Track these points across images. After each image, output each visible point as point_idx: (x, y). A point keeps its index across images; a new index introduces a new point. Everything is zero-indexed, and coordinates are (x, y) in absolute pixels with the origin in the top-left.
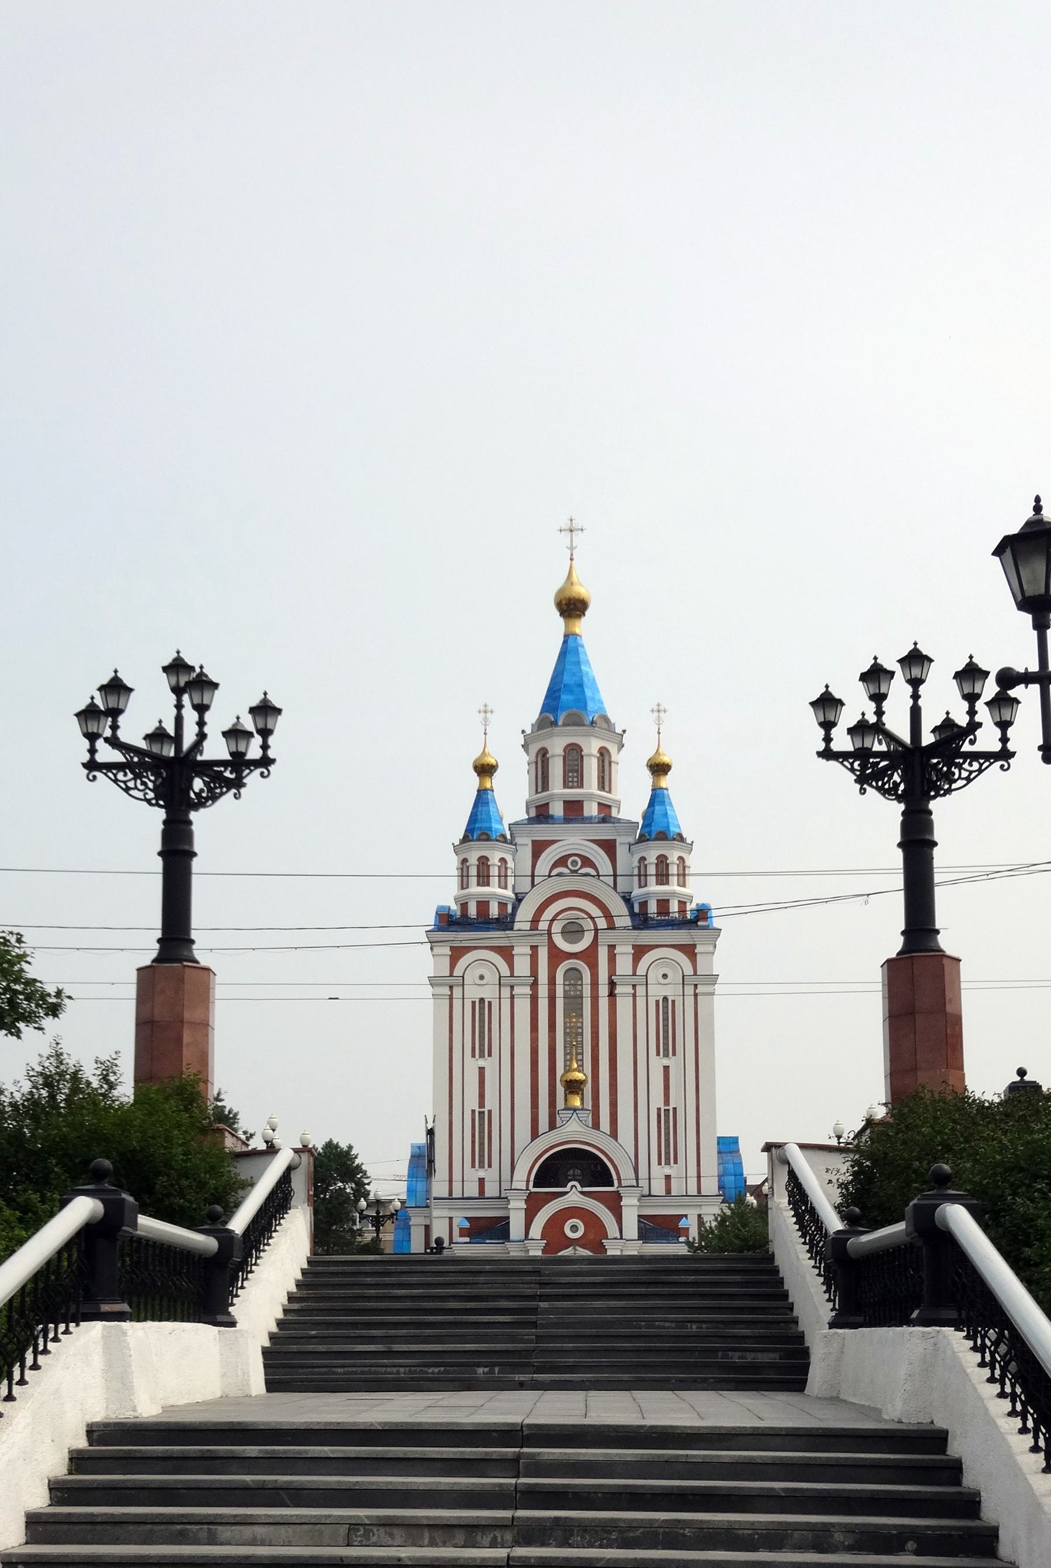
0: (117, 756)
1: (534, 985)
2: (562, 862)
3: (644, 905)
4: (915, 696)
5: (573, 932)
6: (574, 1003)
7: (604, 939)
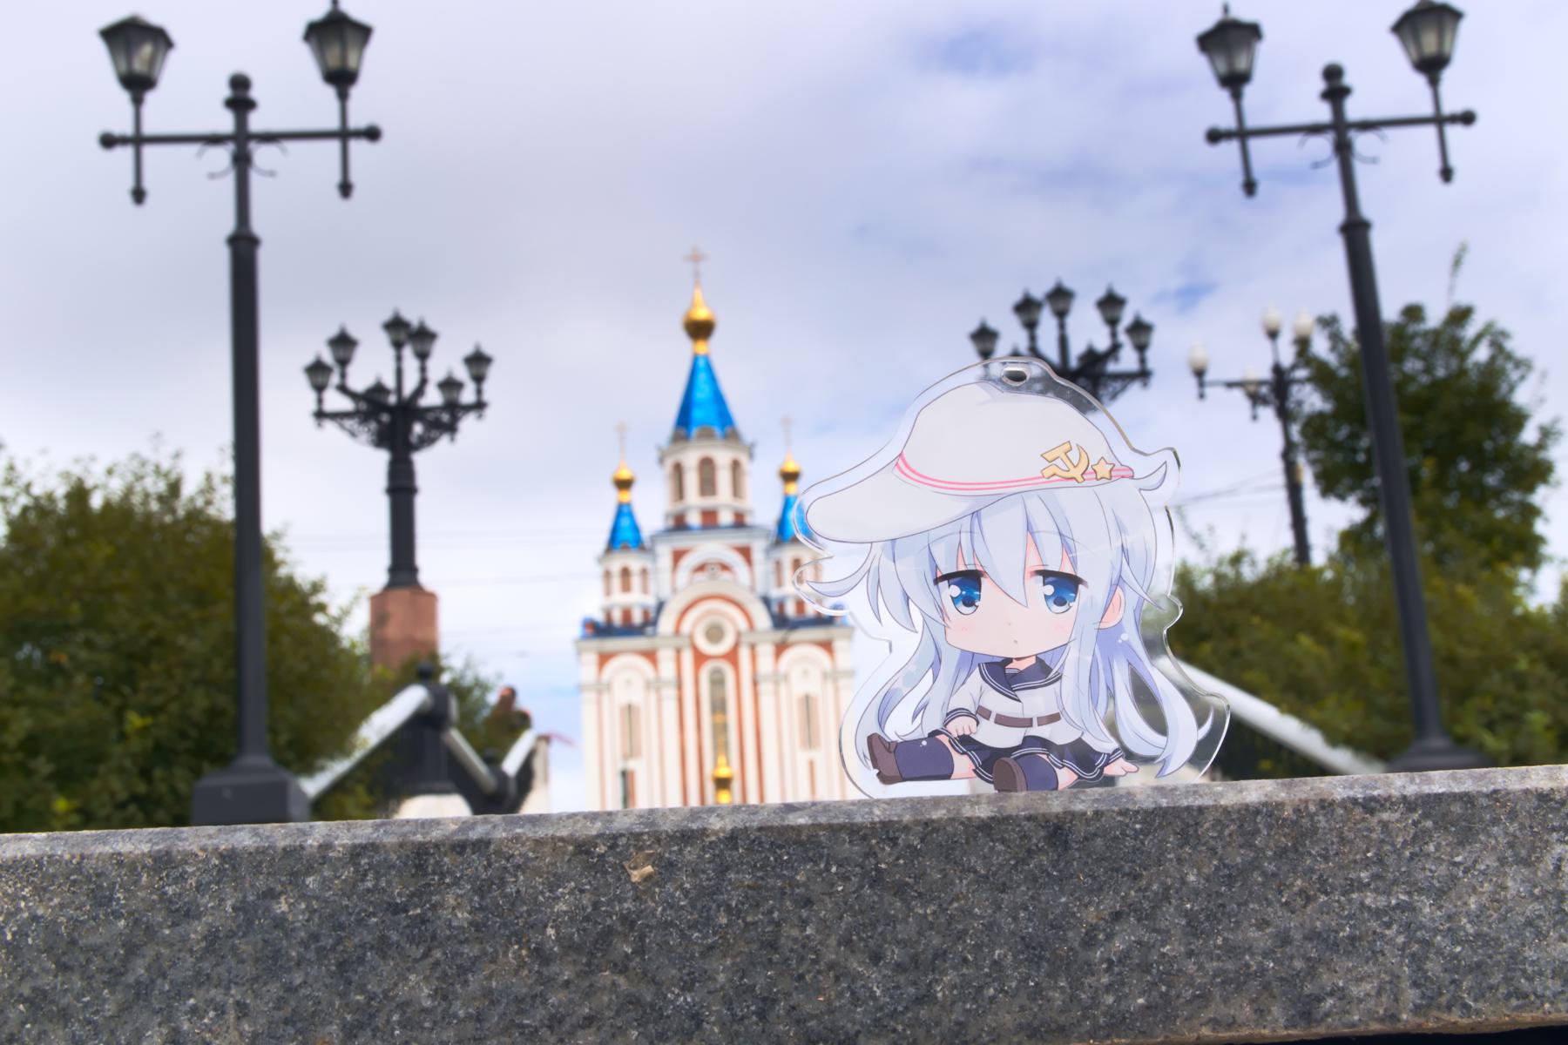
0: (345, 404)
1: (680, 687)
2: (701, 568)
3: (781, 606)
4: (1062, 326)
5: (715, 634)
6: (719, 706)
7: (747, 639)
